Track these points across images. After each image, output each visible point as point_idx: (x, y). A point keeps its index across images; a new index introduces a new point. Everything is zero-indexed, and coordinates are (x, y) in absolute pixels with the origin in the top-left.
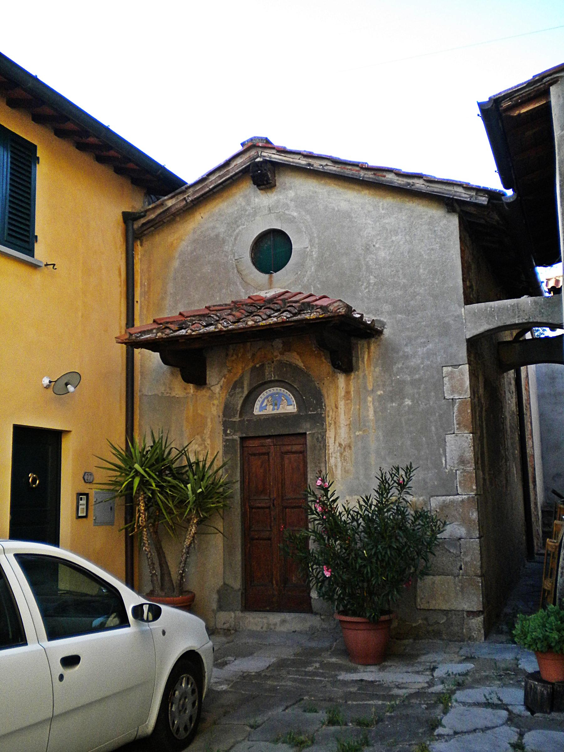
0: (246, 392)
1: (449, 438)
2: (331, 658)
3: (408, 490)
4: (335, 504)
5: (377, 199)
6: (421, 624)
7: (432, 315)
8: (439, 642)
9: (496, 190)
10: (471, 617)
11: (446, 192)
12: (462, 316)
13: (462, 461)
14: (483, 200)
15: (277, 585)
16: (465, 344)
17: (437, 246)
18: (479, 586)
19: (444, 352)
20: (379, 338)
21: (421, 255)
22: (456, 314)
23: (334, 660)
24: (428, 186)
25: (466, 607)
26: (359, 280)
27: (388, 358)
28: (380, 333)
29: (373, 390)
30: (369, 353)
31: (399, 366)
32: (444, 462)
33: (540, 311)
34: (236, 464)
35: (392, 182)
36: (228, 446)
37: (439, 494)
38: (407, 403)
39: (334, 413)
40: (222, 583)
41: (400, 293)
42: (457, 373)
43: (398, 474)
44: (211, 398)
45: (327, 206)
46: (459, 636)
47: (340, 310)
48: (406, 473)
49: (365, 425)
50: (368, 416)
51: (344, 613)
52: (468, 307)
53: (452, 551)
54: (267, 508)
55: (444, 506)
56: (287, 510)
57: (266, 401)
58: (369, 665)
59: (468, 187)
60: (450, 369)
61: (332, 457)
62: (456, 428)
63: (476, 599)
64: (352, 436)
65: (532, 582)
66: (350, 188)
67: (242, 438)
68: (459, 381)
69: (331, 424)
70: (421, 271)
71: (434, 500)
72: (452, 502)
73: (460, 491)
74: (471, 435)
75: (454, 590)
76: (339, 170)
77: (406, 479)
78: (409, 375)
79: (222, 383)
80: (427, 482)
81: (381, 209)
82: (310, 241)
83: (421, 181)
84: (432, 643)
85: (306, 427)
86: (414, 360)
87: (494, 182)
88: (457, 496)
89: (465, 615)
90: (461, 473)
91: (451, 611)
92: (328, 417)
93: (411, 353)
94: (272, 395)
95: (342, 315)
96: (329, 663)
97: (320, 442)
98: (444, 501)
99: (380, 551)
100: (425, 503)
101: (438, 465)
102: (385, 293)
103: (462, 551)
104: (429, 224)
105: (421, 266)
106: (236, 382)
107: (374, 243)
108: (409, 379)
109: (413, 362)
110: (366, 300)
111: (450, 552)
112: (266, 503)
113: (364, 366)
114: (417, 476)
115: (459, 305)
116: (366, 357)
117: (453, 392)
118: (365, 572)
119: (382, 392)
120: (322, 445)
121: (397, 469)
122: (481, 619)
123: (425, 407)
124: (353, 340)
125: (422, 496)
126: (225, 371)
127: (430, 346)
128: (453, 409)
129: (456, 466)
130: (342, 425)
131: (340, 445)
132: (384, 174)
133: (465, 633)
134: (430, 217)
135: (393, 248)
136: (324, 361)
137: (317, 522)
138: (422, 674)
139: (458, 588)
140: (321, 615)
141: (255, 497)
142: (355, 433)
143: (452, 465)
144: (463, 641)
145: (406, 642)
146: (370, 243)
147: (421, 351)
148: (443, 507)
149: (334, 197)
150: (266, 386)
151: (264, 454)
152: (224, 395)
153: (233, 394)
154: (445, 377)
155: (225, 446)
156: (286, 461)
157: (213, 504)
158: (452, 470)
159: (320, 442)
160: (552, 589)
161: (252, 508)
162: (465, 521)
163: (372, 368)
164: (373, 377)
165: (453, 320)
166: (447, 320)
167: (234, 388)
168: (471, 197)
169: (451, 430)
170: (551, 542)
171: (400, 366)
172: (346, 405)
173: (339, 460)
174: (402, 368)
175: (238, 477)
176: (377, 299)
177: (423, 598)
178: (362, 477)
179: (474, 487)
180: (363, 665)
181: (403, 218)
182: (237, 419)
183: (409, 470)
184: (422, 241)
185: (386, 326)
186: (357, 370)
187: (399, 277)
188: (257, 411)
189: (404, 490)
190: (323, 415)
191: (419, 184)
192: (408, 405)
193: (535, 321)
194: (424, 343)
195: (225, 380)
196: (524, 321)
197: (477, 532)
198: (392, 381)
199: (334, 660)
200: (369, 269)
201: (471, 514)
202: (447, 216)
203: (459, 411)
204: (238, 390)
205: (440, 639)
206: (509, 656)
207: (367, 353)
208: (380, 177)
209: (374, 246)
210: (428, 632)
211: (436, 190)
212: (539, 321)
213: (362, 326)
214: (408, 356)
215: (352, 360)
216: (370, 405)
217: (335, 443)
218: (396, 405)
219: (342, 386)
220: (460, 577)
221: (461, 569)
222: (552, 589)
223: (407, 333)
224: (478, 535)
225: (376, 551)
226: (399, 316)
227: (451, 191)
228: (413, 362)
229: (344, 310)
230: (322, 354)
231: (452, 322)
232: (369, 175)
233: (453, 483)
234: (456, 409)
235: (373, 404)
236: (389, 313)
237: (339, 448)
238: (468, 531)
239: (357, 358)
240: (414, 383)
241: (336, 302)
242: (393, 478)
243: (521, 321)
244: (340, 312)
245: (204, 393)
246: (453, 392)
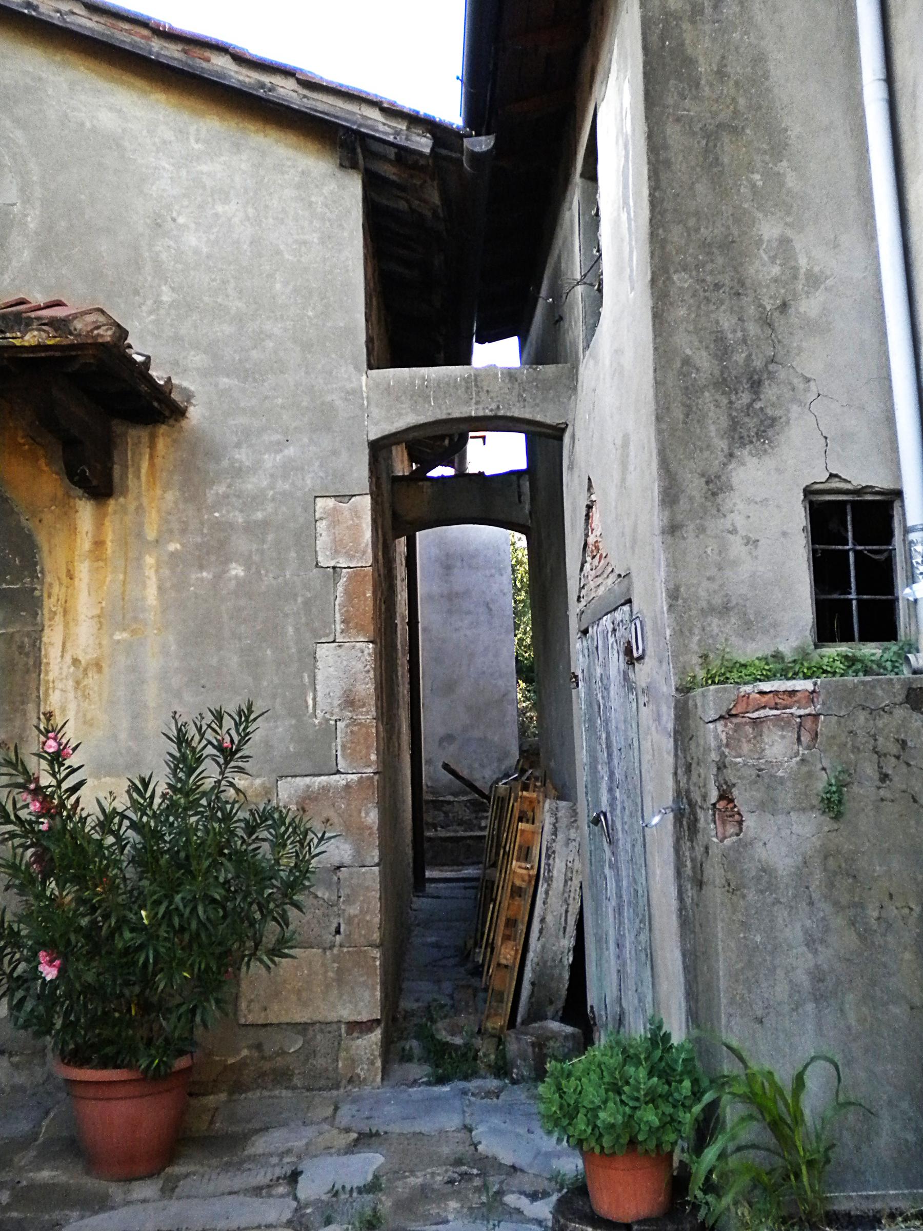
1: (323, 651)
2: (40, 1169)
3: (240, 764)
4: (73, 799)
5: (185, 116)
6: (246, 1057)
7: (297, 385)
8: (284, 1093)
9: (452, 125)
10: (355, 1035)
11: (343, 115)
12: (362, 391)
13: (350, 702)
14: (423, 143)
16: (367, 451)
17: (315, 238)
18: (375, 966)
19: (321, 466)
20: (178, 425)
21: (278, 252)
22: (349, 386)
23: (45, 1175)
24: (305, 96)
25: (346, 1013)
26: (136, 292)
27: (197, 469)
28: (178, 412)
29: (157, 541)
30: (152, 457)
31: (220, 492)
32: (310, 702)
33: (520, 395)
35: (224, 76)
37: (298, 772)
38: (233, 573)
39: (64, 589)
41: (228, 329)
42: (346, 513)
43: (221, 728)
45: (66, 115)
46: (328, 1078)
47: (101, 331)
48: (237, 725)
49: (135, 619)
50: (144, 599)
51: (77, 1058)
52: (374, 373)
53: (320, 894)
55: (306, 800)
58: (136, 1179)
59: (392, 112)
60: (331, 502)
61: (54, 688)
62: (338, 630)
63: (367, 994)
64: (104, 642)
65: (434, 939)
66: (123, 83)
68: (347, 529)
69: (55, 613)
70: (278, 286)
71: (288, 785)
72: (325, 789)
73: (341, 767)
74: (371, 645)
75: (323, 981)
76: (99, 28)
77: (236, 739)
78: (241, 511)
80: (271, 747)
81: (192, 141)
82: (22, 190)
83: (291, 84)
84: (270, 1097)
86: (254, 480)
87: (450, 109)
88: (337, 777)
89: (343, 1031)
90: (347, 726)
91: (313, 1024)
92: (49, 597)
93: (247, 464)
95: (102, 344)
96: (32, 1187)
97: (27, 655)
98: (308, 787)
99: (177, 909)
100: (269, 791)
101: (297, 710)
102: (196, 327)
103: (342, 893)
104: (298, 187)
105: (278, 276)
107: (174, 215)
108: (240, 520)
109: (250, 485)
110: (149, 338)
111: (316, 897)
113: (140, 486)
114: (260, 731)
115: (357, 368)
116: (145, 465)
117: (336, 553)
118: (141, 960)
119: (178, 546)
120: (31, 662)
121: (219, 716)
122: (376, 1036)
123: (274, 582)
124: (118, 427)
125: (258, 776)
127: (290, 451)
128: (335, 590)
129: (337, 710)
130: (83, 617)
131: (76, 662)
132: (207, 54)
133: (340, 1071)
134: (303, 173)
135: (215, 230)
136: (45, 469)
137: (17, 841)
138: (270, 1196)
139: (331, 974)
140: (11, 1055)
142: (111, 635)
143: (328, 709)
144: (337, 1086)
145: (211, 1100)
146: (163, 212)
147: (270, 461)
148: (304, 799)
149: (83, 97)
154: (321, 519)
158: (328, 720)
159: (27, 655)
160: (514, 963)
162: (354, 831)
163: (159, 492)
164: (158, 511)
165: (341, 398)
166: (329, 398)
168: (397, 133)
169: (328, 635)
170: (520, 867)
171: (221, 489)
172: (94, 571)
173: (71, 695)
174: (226, 496)
176: (177, 339)
177: (252, 1001)
178: (123, 736)
179: (373, 757)
180: (119, 1180)
181: (243, 166)
183: (245, 716)
184: (282, 221)
185: (193, 401)
186: (124, 492)
187: (227, 296)
189: (232, 764)
190: (37, 593)
191: (286, 91)
192: (236, 576)
193: (509, 414)
194: (279, 443)
196: (488, 413)
197: (376, 853)
198: (202, 524)
199: (45, 1175)
200: (160, 271)
201: (363, 814)
202: (339, 174)
203: (350, 594)
205: (287, 1088)
206: (451, 1122)
207: (147, 456)
208: (198, 61)
209: (174, 220)
210: (263, 1074)
211: (320, 107)
212: (516, 415)
213: (144, 388)
214: (240, 469)
215: (111, 469)
216: (151, 573)
217: (62, 656)
218: (210, 576)
219: (85, 529)
220: (335, 950)
221: (338, 932)
222: (514, 963)
223: (242, 420)
224: (376, 860)
225: (167, 907)
226: (226, 380)
227: (354, 114)
228: (250, 485)
229: (110, 333)
230: (41, 452)
231: (338, 403)
232: (172, 53)
233: (330, 748)
234: (340, 589)
235: (157, 571)
236: (205, 373)
237: (72, 669)
238: (358, 852)
239: (125, 467)
240: (255, 530)
241: (89, 312)
242: (202, 736)
243: (481, 413)
244: (98, 335)
246: (336, 553)
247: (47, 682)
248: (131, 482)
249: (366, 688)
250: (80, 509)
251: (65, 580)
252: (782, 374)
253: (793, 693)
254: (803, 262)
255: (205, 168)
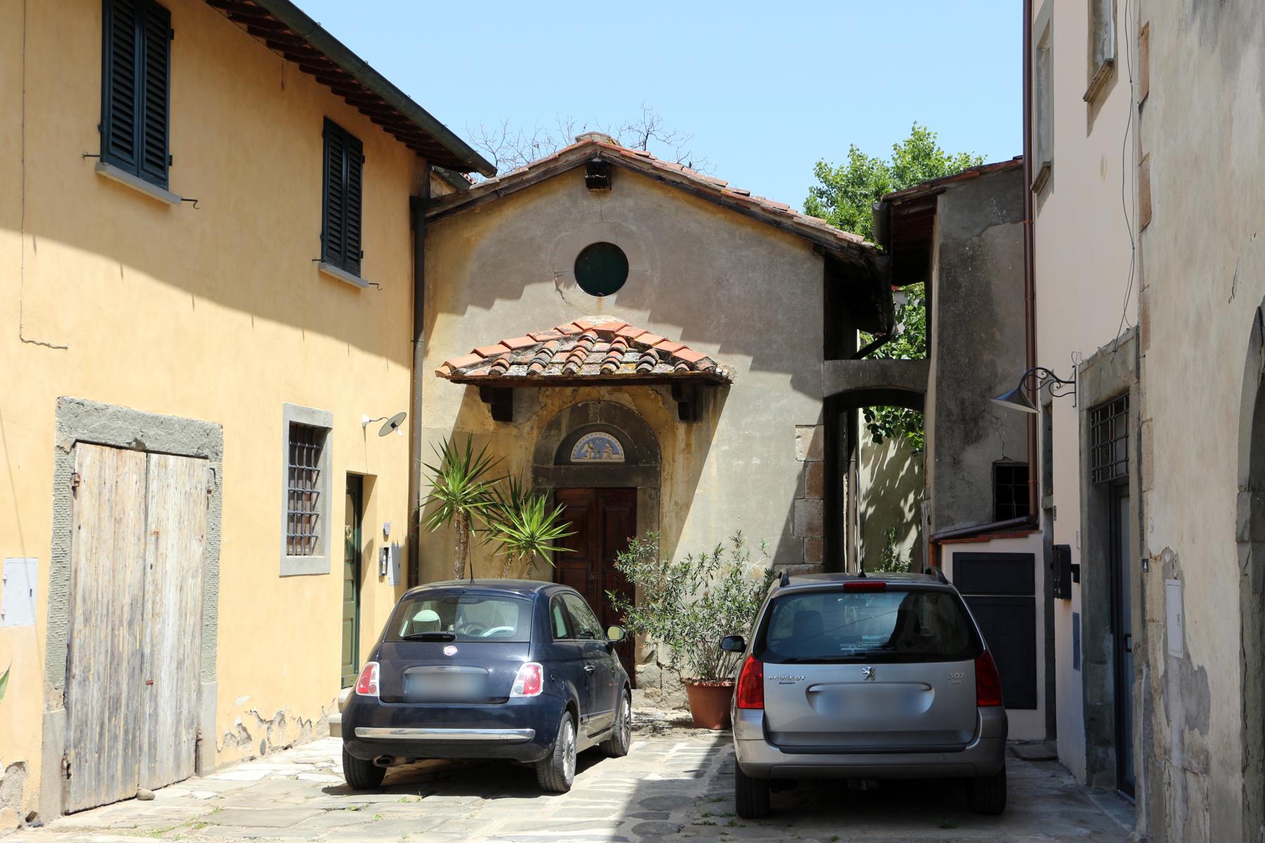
13: (811, 528)
85: (637, 481)
94: (593, 441)
116: (711, 406)
131: (676, 503)
204: (553, 432)
248: (705, 415)
249: (819, 521)
252: (988, 417)
253: (150, 732)
254: (1000, 370)
255: (744, 253)
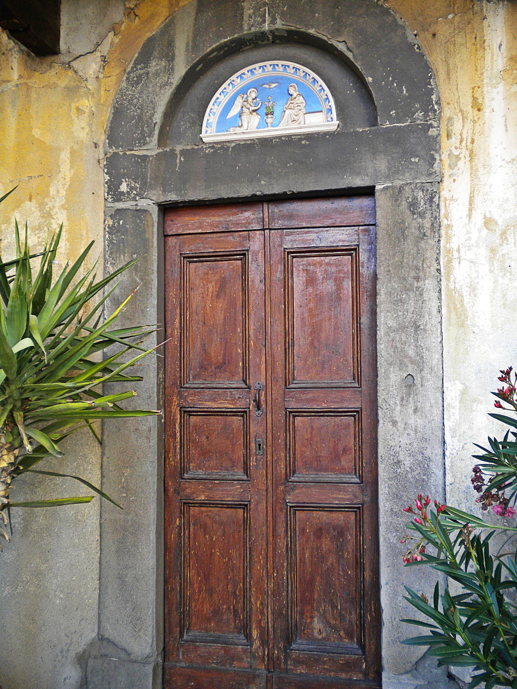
0: (181, 69)
15: (264, 643)
34: (146, 284)
36: (121, 227)
39: (469, 125)
40: (94, 635)
44: (72, 92)
54: (234, 413)
56: (298, 419)
57: (239, 102)
67: (167, 209)
69: (458, 158)
79: (105, 48)
92: (449, 136)
94: (258, 85)
97: (422, 215)
106: (151, 40)
112: (233, 400)
126: (117, 14)
141: (198, 383)
150: (239, 58)
151: (227, 256)
152: (113, 82)
153: (140, 77)
155: (111, 230)
156: (298, 281)
157: (76, 398)
159: (422, 215)
161: (190, 413)
167: (145, 57)
175: (151, 319)
182: (151, 149)
188: (211, 132)
190: (432, 132)
195: (117, 40)
204: (154, 66)
217: (470, 216)
237: (485, 232)
245: (54, 76)
247: (449, 251)
250: (490, 16)
251: (468, 109)
